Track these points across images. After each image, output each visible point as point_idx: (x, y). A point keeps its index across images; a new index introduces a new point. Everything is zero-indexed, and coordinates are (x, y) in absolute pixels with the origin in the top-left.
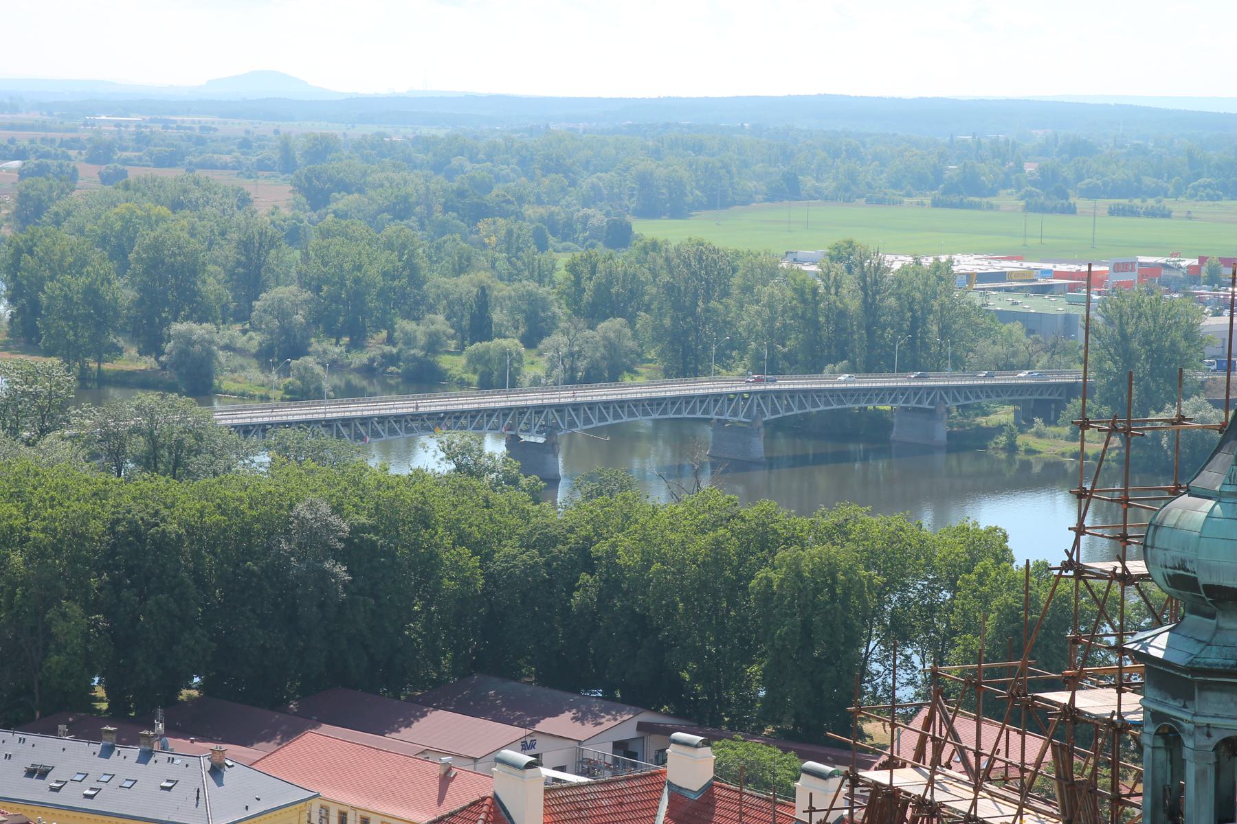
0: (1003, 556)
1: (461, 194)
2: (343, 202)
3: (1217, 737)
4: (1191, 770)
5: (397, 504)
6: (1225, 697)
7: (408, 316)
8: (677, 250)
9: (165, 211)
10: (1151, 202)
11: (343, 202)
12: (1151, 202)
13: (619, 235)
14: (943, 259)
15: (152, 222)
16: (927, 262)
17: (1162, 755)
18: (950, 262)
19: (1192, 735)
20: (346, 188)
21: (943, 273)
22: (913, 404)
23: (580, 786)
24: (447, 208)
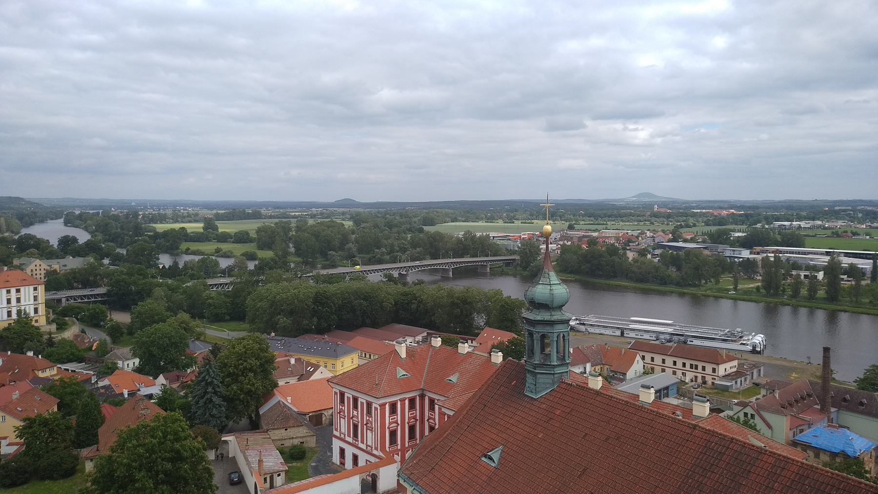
0: (49, 243)
1: (388, 222)
2: (363, 225)
3: (540, 334)
4: (535, 342)
5: (19, 252)
6: (542, 326)
7: (377, 249)
8: (433, 233)
9: (326, 228)
10: (529, 221)
11: (363, 225)
12: (529, 221)
13: (421, 231)
14: (488, 234)
15: (324, 230)
16: (485, 234)
17: (529, 339)
18: (489, 234)
19: (535, 334)
20: (363, 222)
21: (488, 236)
22: (482, 264)
23: (415, 346)
24: (385, 226)
